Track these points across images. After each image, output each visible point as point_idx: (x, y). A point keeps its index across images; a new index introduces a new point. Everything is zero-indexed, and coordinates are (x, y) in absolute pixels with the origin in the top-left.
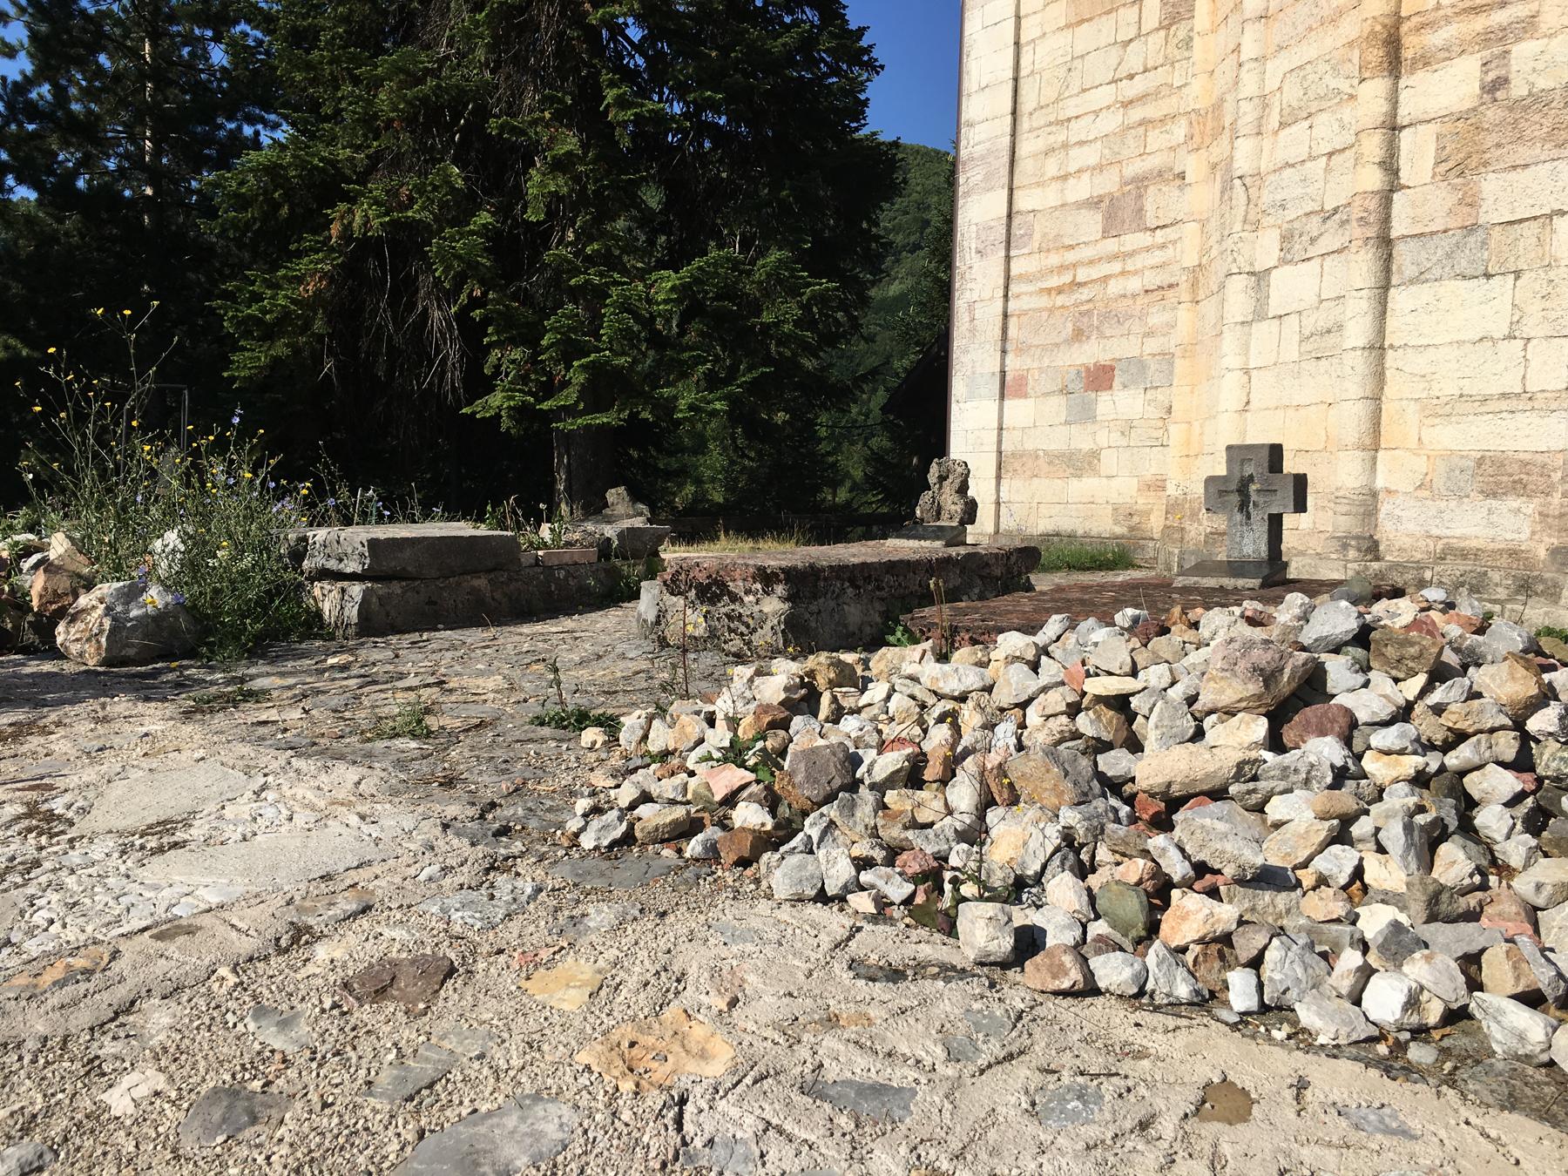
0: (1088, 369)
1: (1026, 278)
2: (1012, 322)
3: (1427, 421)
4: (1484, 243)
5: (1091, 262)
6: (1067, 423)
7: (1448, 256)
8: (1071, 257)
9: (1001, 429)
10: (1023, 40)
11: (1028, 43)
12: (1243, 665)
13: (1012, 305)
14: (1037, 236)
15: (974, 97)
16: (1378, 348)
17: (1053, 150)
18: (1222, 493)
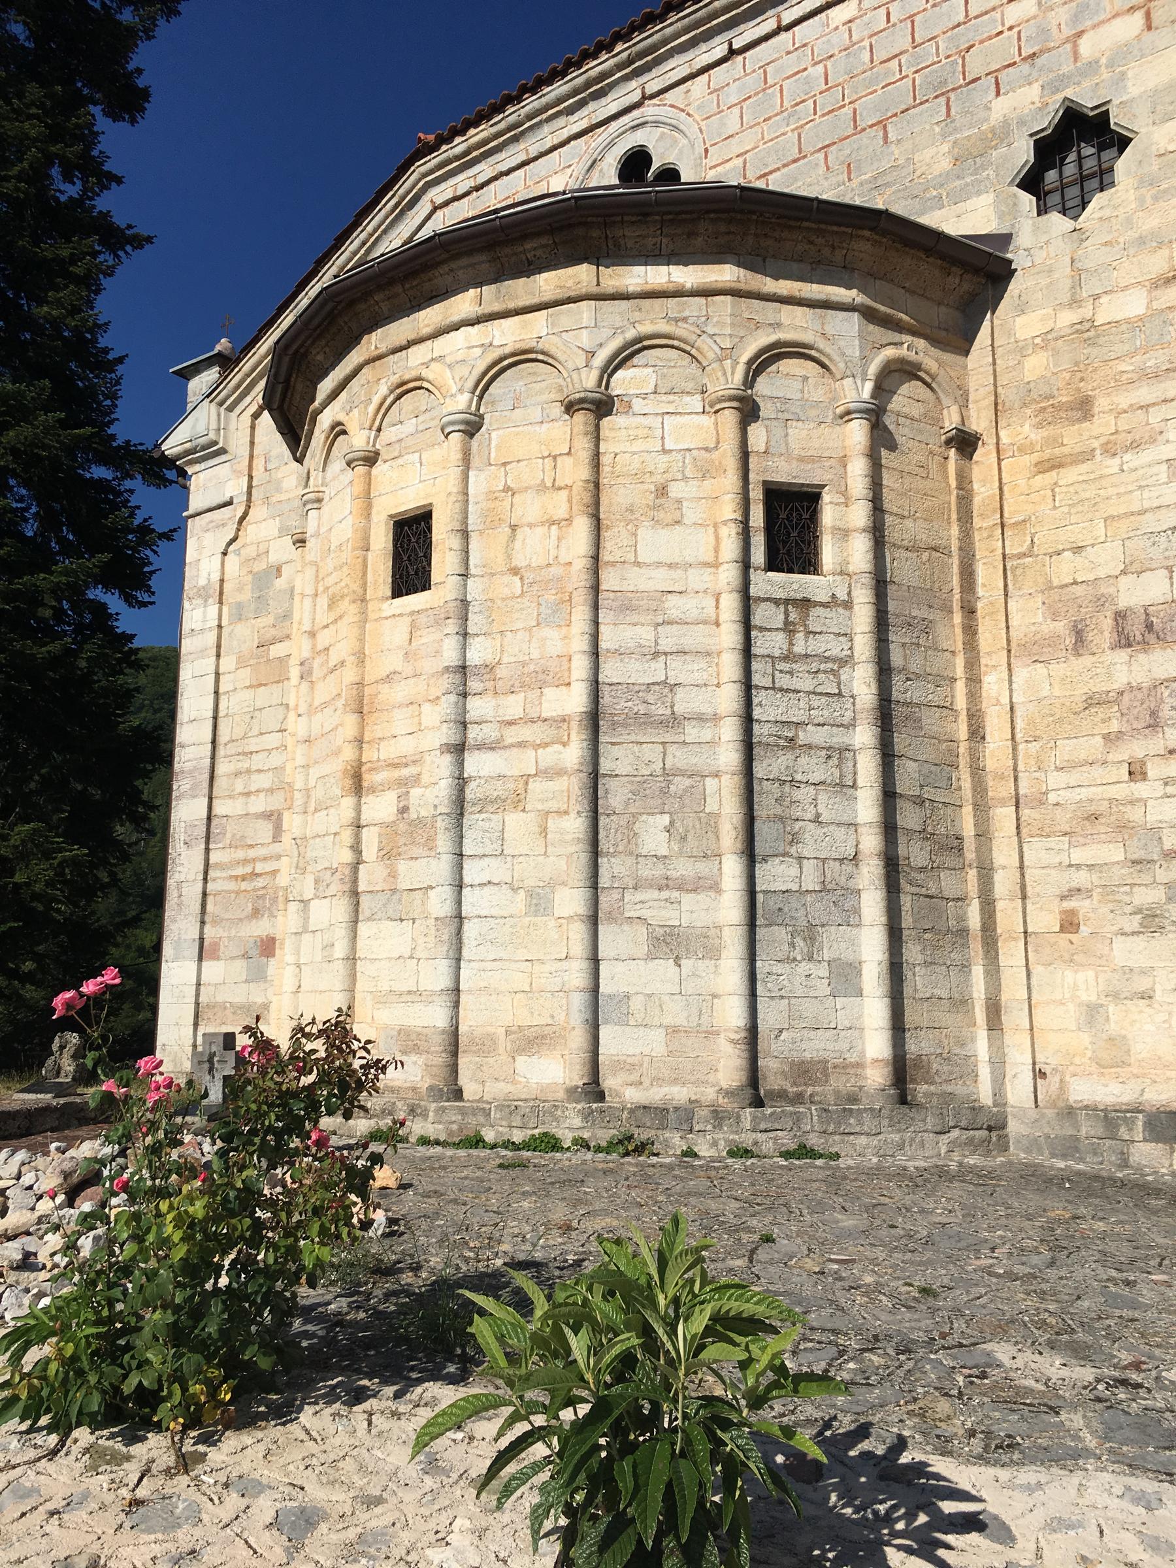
0: (262, 940)
1: (221, 866)
2: (210, 900)
3: (377, 1006)
4: (400, 900)
5: (265, 859)
6: (246, 981)
7: (384, 905)
8: (252, 853)
9: (199, 984)
10: (221, 690)
11: (225, 693)
12: (58, 1170)
13: (210, 886)
14: (229, 835)
15: (185, 726)
16: (352, 959)
17: (241, 773)
18: (200, 1063)
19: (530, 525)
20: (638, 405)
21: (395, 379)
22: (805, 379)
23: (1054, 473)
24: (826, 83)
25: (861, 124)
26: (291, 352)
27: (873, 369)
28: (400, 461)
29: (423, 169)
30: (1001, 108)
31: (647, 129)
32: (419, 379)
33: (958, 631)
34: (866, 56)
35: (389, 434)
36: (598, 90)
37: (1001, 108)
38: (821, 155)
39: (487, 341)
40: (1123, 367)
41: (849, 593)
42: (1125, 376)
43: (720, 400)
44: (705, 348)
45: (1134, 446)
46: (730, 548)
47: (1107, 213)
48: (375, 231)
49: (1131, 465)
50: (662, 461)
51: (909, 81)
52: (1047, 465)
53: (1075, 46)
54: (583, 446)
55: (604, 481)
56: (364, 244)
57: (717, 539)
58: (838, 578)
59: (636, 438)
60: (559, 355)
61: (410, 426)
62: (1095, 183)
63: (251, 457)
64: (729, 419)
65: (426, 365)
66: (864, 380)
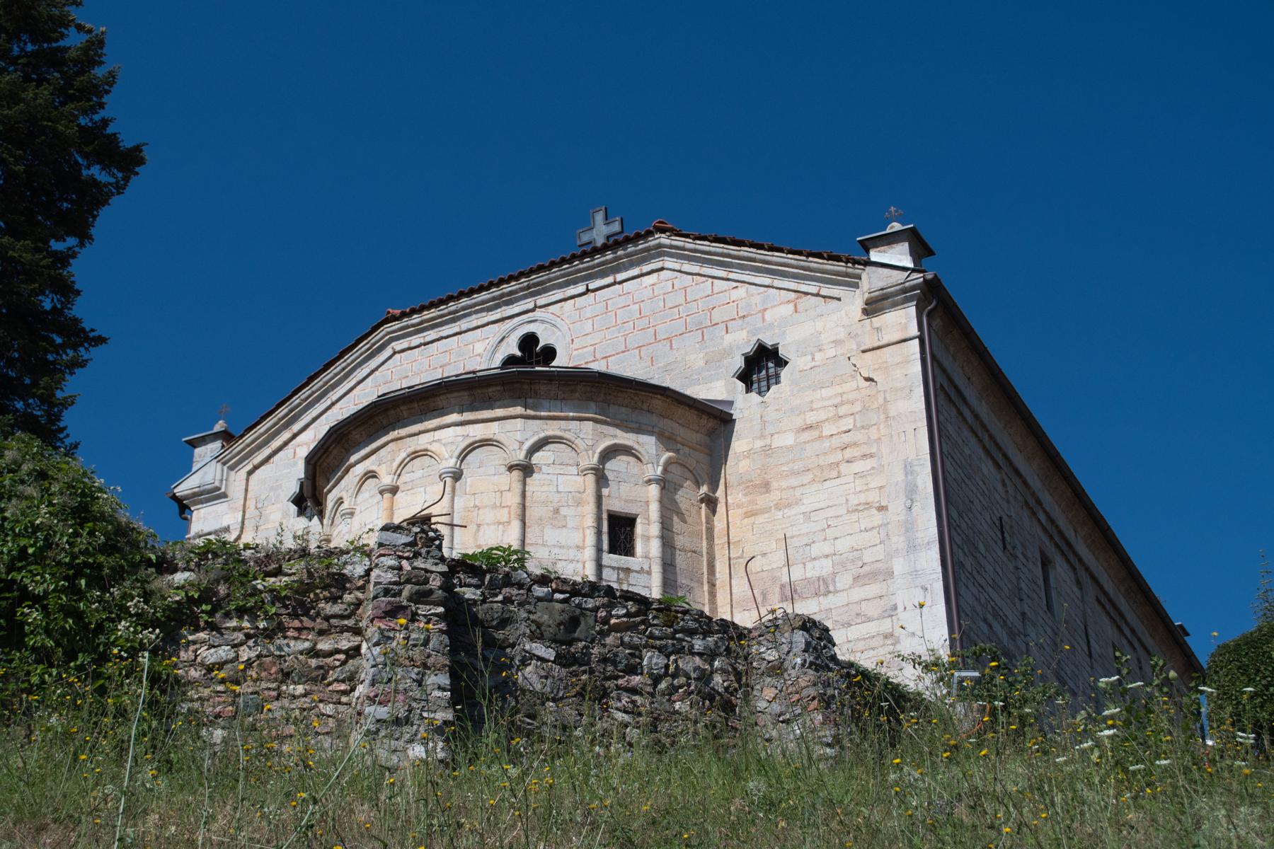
19: (488, 524)
20: (545, 469)
21: (411, 450)
22: (629, 463)
23: (753, 518)
24: (640, 314)
25: (659, 338)
26: (338, 433)
27: (662, 461)
28: (412, 491)
29: (389, 330)
30: (728, 339)
31: (537, 324)
32: (426, 450)
33: (706, 594)
34: (661, 304)
35: (405, 477)
36: (509, 300)
37: (728, 339)
38: (637, 351)
39: (466, 434)
40: (784, 468)
41: (650, 567)
42: (785, 473)
43: (586, 470)
44: (579, 445)
45: (789, 506)
46: (590, 539)
47: (777, 395)
48: (352, 362)
49: (788, 514)
50: (556, 497)
51: (683, 320)
52: (750, 514)
53: (763, 315)
54: (517, 487)
55: (527, 504)
56: (344, 369)
57: (584, 536)
58: (645, 560)
59: (544, 485)
60: (505, 443)
61: (419, 473)
62: (774, 381)
63: (245, 499)
64: (591, 479)
65: (430, 443)
66: (658, 466)
